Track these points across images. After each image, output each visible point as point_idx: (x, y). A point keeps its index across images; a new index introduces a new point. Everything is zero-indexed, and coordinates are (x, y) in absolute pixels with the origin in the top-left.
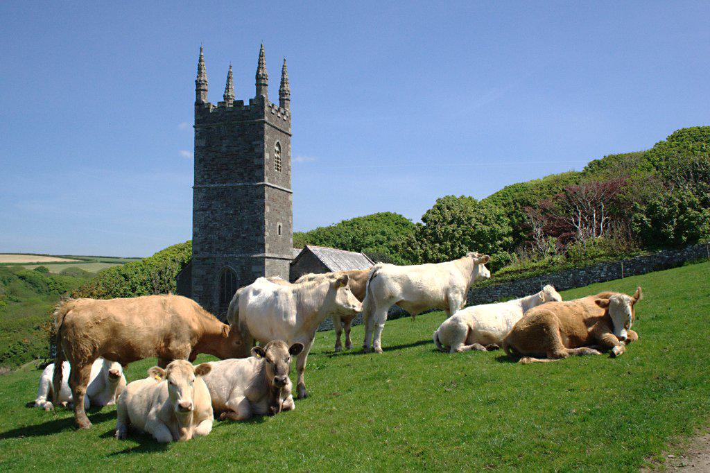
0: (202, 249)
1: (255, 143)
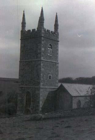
0: (21, 84)
1: (38, 44)
